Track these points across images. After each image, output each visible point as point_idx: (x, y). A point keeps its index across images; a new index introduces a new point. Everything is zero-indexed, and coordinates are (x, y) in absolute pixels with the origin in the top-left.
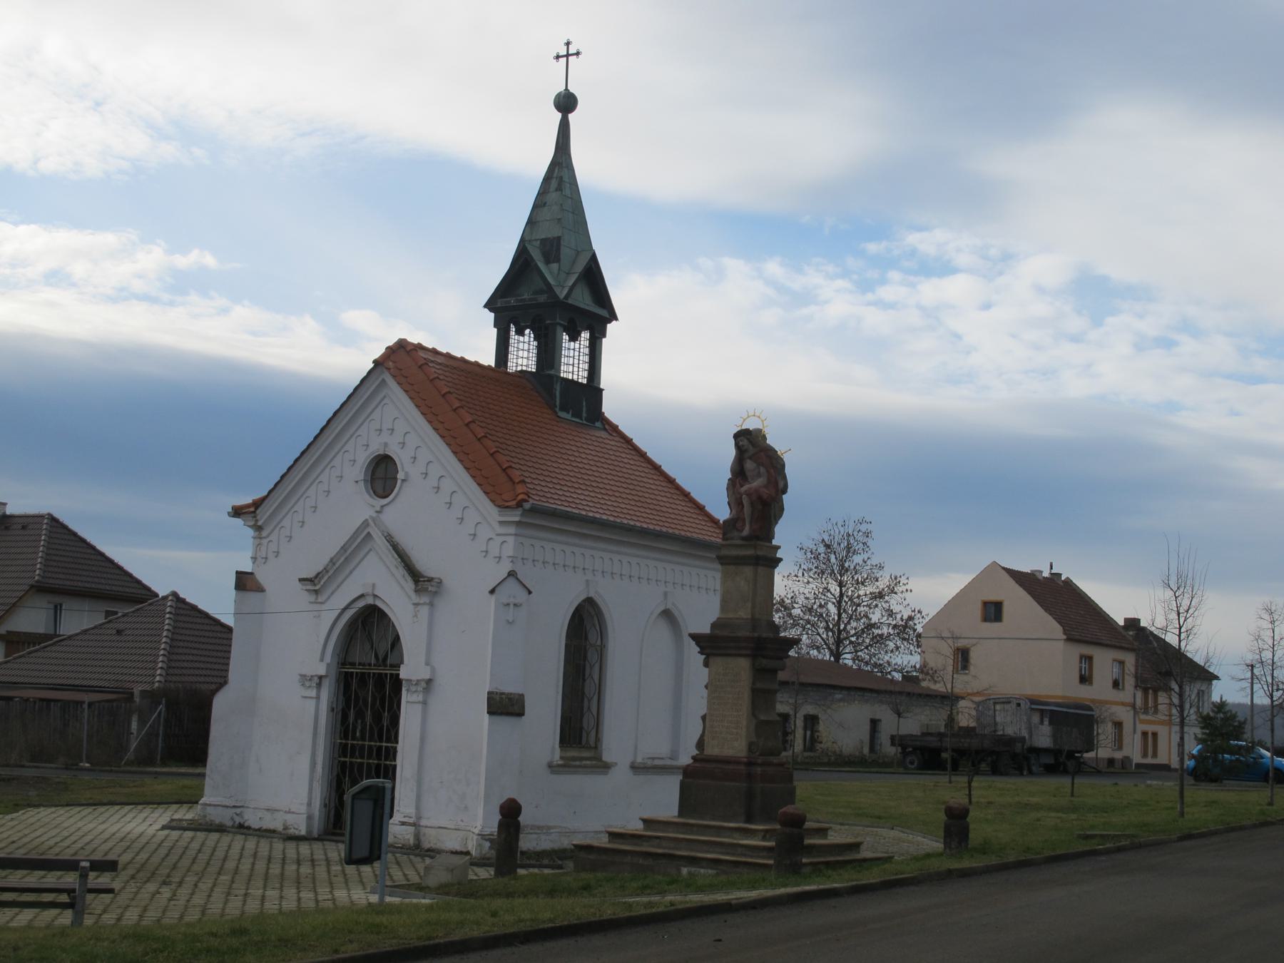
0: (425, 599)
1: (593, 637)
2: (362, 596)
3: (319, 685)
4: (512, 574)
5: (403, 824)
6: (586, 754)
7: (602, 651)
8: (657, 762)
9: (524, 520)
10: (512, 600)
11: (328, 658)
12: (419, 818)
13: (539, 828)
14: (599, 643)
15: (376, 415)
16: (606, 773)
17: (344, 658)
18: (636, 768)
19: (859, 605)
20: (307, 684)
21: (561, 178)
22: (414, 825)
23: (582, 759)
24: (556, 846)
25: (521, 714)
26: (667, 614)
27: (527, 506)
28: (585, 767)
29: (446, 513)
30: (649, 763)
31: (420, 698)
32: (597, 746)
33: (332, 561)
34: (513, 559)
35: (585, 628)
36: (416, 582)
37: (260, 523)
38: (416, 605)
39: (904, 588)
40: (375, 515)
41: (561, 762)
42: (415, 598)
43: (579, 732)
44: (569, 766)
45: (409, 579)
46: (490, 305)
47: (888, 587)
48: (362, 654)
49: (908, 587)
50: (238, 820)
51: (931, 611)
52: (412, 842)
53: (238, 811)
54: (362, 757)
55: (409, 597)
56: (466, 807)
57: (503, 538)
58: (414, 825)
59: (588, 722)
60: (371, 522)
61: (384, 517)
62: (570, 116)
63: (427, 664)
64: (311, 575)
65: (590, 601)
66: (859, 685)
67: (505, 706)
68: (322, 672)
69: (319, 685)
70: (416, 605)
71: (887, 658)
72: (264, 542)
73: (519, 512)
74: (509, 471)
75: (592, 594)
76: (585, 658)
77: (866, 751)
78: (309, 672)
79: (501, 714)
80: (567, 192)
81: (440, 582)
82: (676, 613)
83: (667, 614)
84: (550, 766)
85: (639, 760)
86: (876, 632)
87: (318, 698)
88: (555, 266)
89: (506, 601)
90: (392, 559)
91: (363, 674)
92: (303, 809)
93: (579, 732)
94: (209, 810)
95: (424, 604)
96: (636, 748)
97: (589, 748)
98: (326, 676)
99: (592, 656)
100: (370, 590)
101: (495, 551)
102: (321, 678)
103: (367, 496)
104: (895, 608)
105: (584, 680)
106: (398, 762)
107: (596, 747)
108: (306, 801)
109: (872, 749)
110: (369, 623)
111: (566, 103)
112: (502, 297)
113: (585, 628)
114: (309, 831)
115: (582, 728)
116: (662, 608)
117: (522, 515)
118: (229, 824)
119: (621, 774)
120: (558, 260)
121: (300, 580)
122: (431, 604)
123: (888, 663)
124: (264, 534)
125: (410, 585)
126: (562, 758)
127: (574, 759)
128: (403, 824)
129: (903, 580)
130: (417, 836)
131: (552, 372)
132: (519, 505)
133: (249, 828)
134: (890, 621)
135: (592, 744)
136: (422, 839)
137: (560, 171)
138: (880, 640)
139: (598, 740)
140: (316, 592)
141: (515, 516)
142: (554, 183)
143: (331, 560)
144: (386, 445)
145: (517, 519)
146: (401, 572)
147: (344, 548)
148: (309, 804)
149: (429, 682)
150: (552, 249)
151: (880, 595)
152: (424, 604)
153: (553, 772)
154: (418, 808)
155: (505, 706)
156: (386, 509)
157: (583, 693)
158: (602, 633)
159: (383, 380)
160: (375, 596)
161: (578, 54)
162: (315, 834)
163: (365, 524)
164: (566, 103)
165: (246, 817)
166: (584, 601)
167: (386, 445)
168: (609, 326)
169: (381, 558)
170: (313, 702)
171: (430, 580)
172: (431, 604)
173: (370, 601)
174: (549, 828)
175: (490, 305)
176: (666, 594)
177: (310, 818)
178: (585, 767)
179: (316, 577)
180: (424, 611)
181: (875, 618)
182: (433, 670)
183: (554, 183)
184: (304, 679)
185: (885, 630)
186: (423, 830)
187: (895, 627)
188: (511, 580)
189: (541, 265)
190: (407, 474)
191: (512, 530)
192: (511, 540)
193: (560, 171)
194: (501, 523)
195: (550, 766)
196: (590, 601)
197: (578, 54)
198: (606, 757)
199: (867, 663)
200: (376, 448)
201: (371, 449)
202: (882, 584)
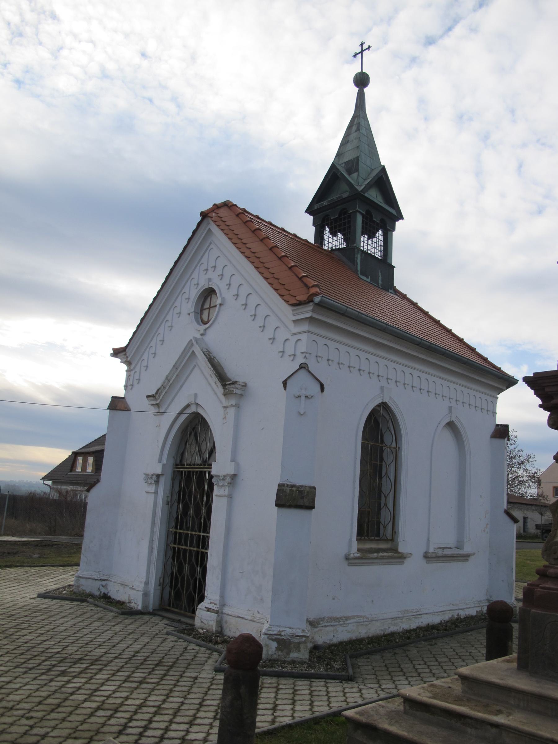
0: (233, 402)
1: (388, 439)
2: (188, 406)
3: (157, 482)
4: (303, 366)
5: (208, 610)
6: (383, 546)
7: (397, 452)
8: (447, 552)
9: (315, 316)
10: (303, 393)
11: (164, 461)
12: (223, 605)
13: (336, 619)
14: (394, 445)
15: (204, 260)
16: (402, 563)
17: (179, 460)
18: (427, 557)
19: (513, 467)
20: (150, 481)
21: (359, 123)
22: (217, 612)
23: (378, 551)
24: (354, 636)
25: (312, 507)
26: (451, 426)
27: (317, 299)
28: (382, 558)
29: (260, 332)
30: (440, 552)
31: (226, 493)
32: (393, 539)
33: (167, 379)
34: (305, 354)
35: (379, 431)
36: (224, 386)
37: (128, 359)
38: (225, 407)
39: (532, 460)
40: (198, 336)
41: (357, 555)
42: (225, 403)
43: (375, 524)
44: (366, 558)
45: (219, 384)
46: (309, 211)
47: (526, 459)
48: (193, 458)
49: (535, 459)
50: (103, 590)
51: (543, 470)
52: (214, 629)
53: (104, 583)
54: (186, 545)
55: (221, 402)
56: (262, 599)
57: (298, 337)
58: (217, 612)
59: (385, 516)
60: (193, 341)
61: (207, 338)
62: (365, 90)
63: (233, 460)
64: (153, 393)
65: (384, 406)
66: (518, 501)
67: (295, 499)
68: (159, 471)
69: (157, 482)
70: (225, 407)
71: (525, 491)
72: (132, 372)
73: (310, 307)
74: (305, 279)
75: (386, 400)
76: (382, 459)
77: (522, 531)
78: (151, 471)
79: (290, 506)
80: (363, 131)
81: (245, 385)
82: (459, 425)
83: (451, 426)
84: (347, 558)
85: (431, 550)
86: (520, 479)
87: (156, 493)
88: (355, 175)
89: (297, 394)
90: (208, 370)
91: (189, 472)
92: (142, 587)
93: (375, 524)
94: (82, 581)
95: (231, 406)
96: (428, 540)
97: (386, 540)
98: (162, 475)
99: (388, 457)
100: (192, 400)
101: (290, 350)
102: (158, 476)
103: (195, 323)
104: (529, 469)
105: (381, 478)
106: (209, 552)
107: (392, 540)
108: (144, 580)
109: (524, 531)
110: (193, 430)
111: (362, 81)
112: (318, 202)
113: (379, 431)
114: (145, 606)
115: (379, 523)
116: (448, 420)
117: (313, 311)
118: (97, 593)
119: (414, 564)
120: (357, 170)
121: (148, 397)
122: (237, 406)
123: (526, 493)
124: (132, 367)
125: (220, 390)
126: (359, 550)
127: (371, 551)
128: (208, 610)
129: (532, 456)
130: (220, 623)
131: (354, 245)
132: (310, 300)
133: (110, 598)
134: (527, 474)
135: (389, 537)
136: (225, 626)
137: (359, 128)
138: (522, 483)
139: (394, 532)
140: (158, 405)
141: (307, 312)
142: (354, 128)
143: (167, 378)
144: (210, 280)
145: (308, 315)
146: (214, 380)
147: (175, 367)
148: (147, 583)
149: (234, 477)
150: (353, 166)
151: (523, 463)
152: (231, 406)
153: (350, 564)
154: (222, 596)
155: (295, 499)
156: (208, 331)
157: (380, 491)
158: (397, 436)
159: (209, 229)
160: (197, 404)
161: (369, 48)
162: (151, 609)
163: (190, 344)
164: (362, 81)
165: (109, 589)
166: (379, 406)
167: (210, 280)
168: (397, 223)
169: (203, 373)
170: (153, 496)
171: (235, 383)
172: (237, 406)
173: (193, 409)
174: (347, 618)
175: (309, 211)
176: (450, 408)
177: (146, 595)
178: (382, 558)
179: (157, 393)
180: (232, 411)
181: (520, 472)
182: (238, 466)
183: (354, 128)
184: (148, 477)
185: (525, 478)
186: (226, 618)
187: (530, 476)
188: (303, 372)
189: (346, 175)
190: (223, 299)
191: (305, 327)
192: (304, 337)
193: (359, 128)
194: (294, 321)
195: (347, 558)
196: (384, 406)
197: (369, 48)
198: (401, 549)
199: (517, 493)
200: (203, 284)
201: (200, 286)
202: (522, 459)
